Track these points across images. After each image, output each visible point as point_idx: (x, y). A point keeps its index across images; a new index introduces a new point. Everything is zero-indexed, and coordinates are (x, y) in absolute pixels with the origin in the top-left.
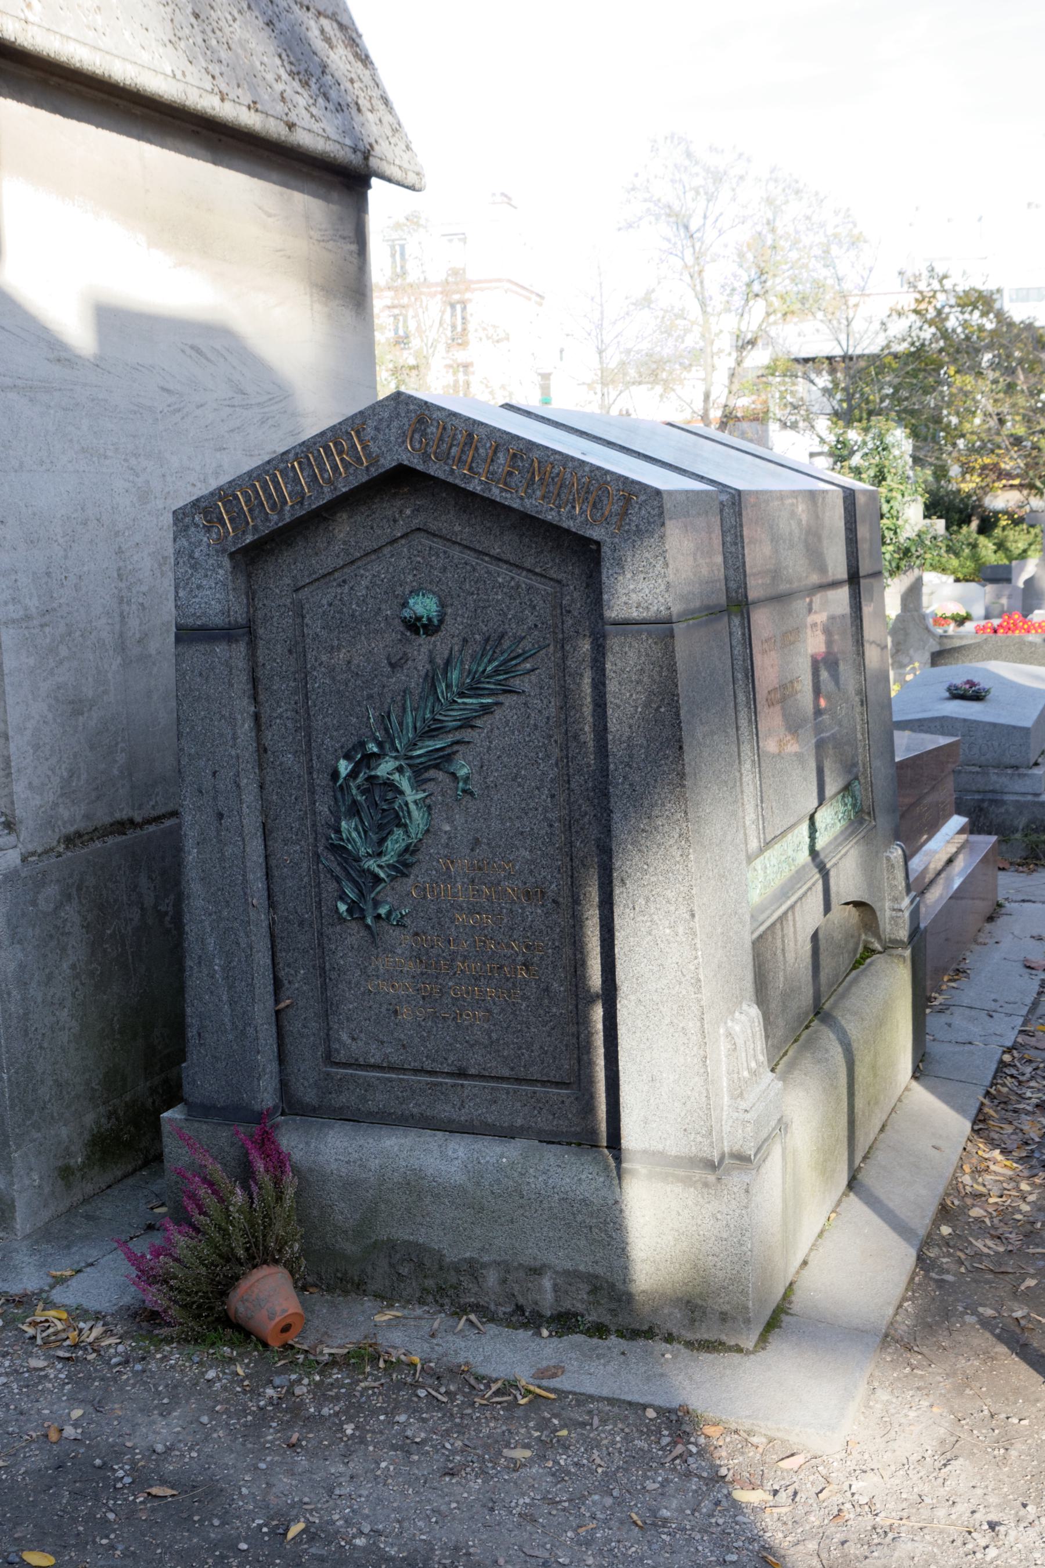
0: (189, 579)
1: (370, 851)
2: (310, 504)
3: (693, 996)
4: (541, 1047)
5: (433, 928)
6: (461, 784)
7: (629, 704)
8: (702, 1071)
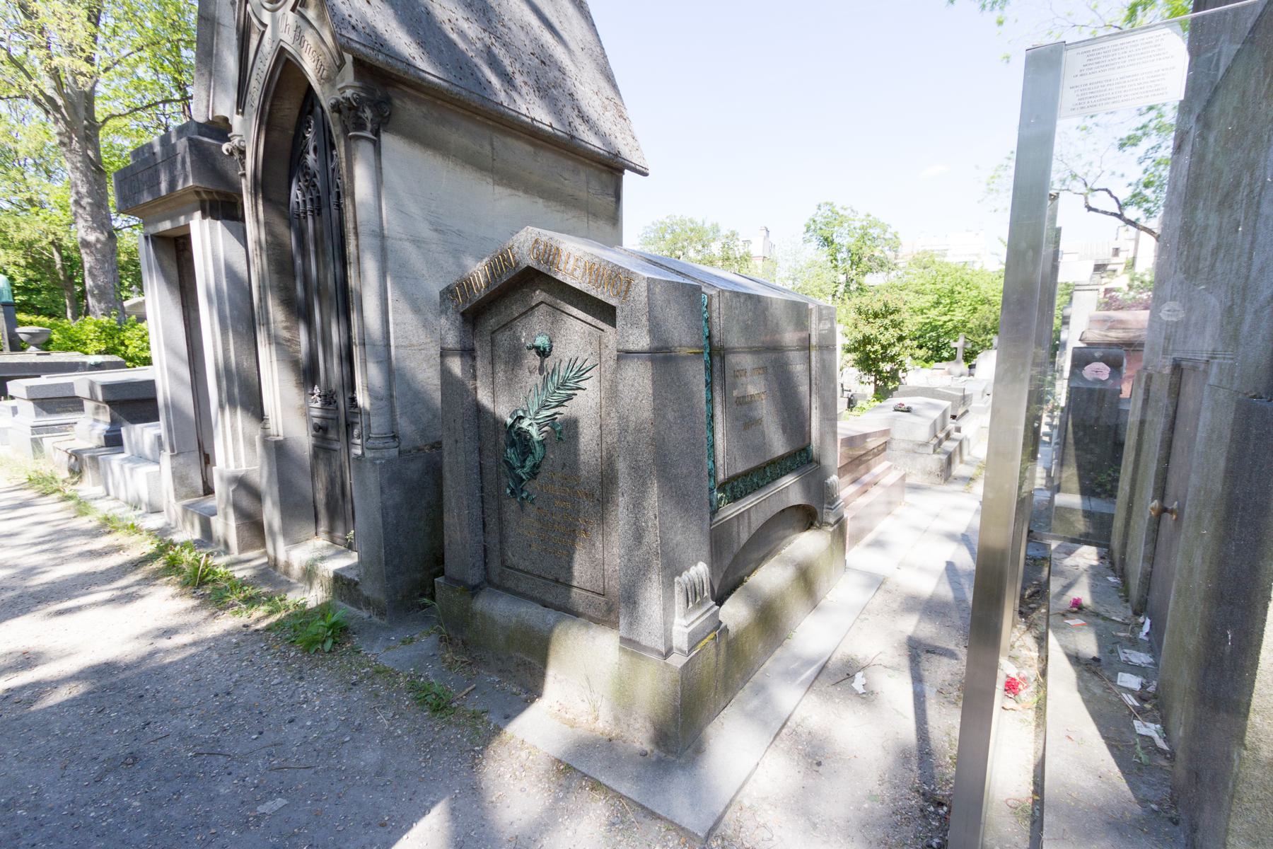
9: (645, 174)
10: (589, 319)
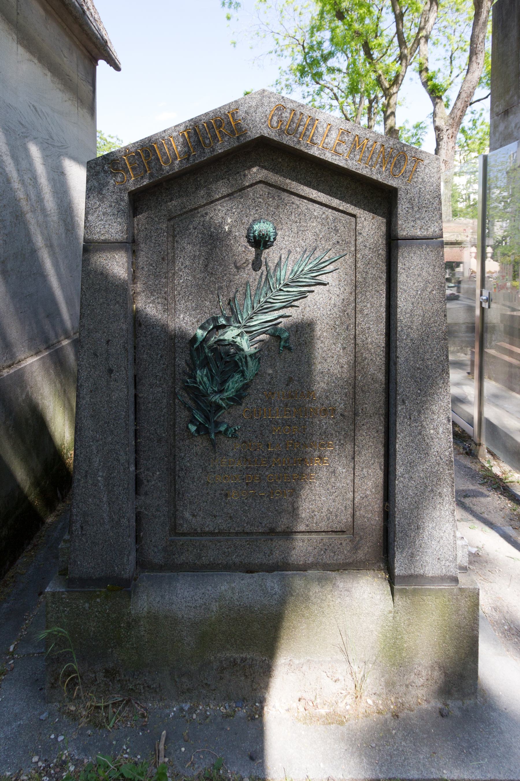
0: (97, 208)
1: (216, 389)
2: (194, 160)
3: (447, 472)
4: (328, 509)
5: (256, 437)
6: (282, 343)
7: (413, 289)
8: (451, 519)
9: (117, 68)
10: (335, 202)
